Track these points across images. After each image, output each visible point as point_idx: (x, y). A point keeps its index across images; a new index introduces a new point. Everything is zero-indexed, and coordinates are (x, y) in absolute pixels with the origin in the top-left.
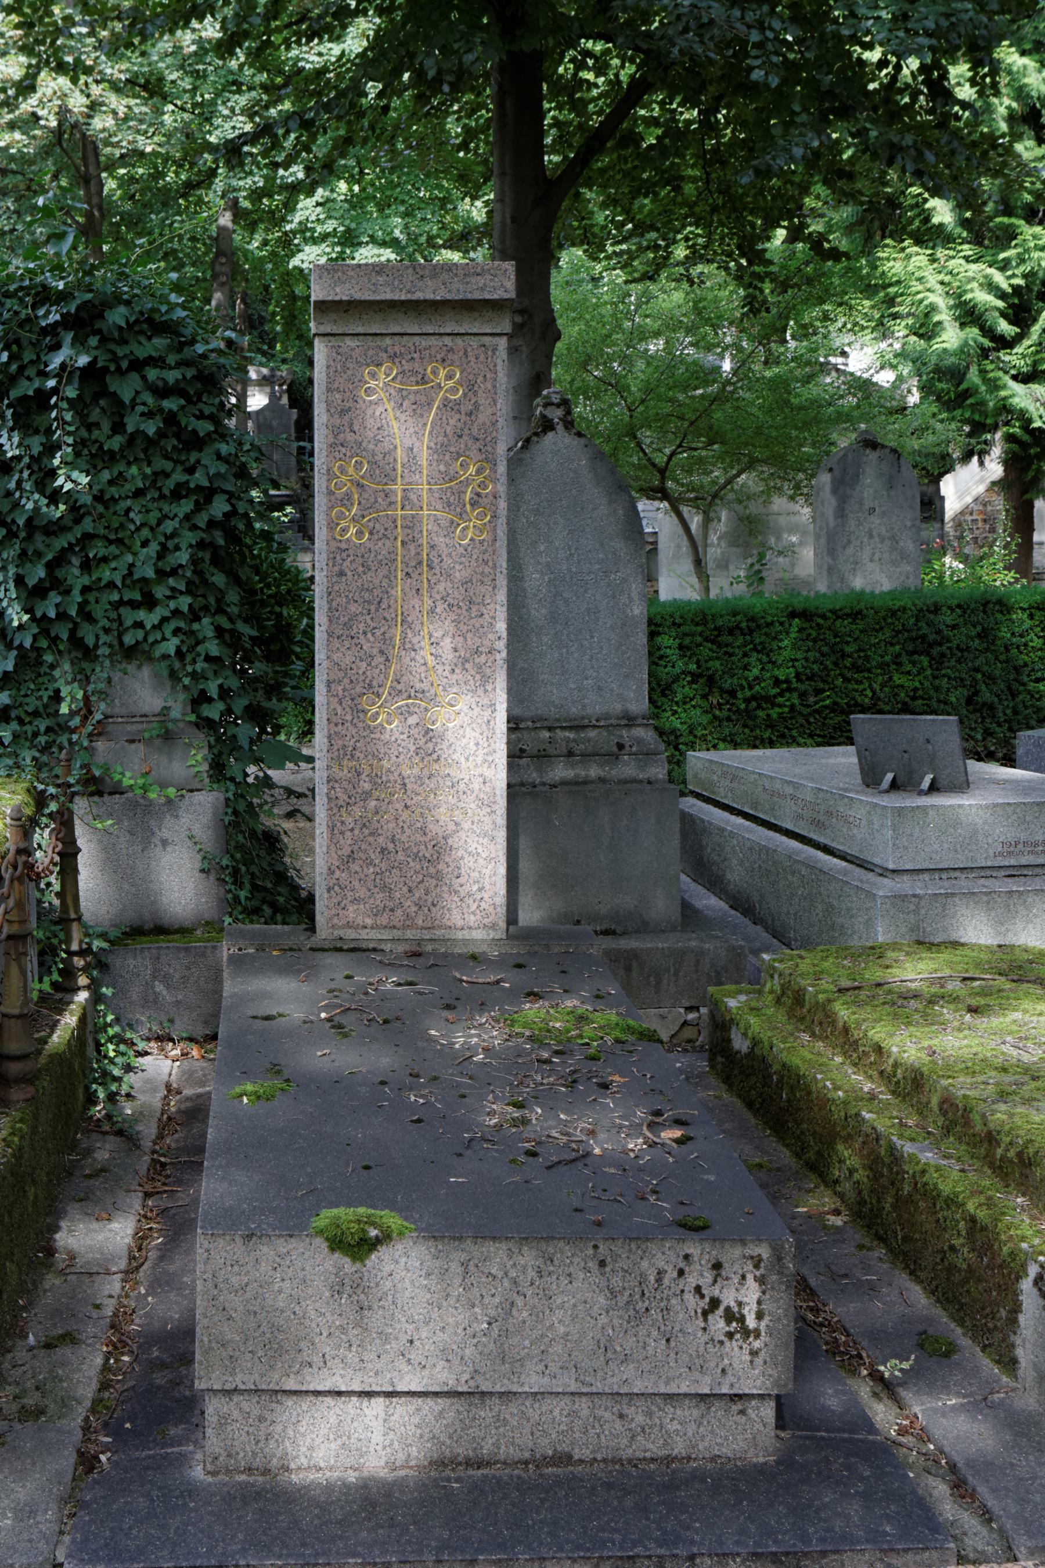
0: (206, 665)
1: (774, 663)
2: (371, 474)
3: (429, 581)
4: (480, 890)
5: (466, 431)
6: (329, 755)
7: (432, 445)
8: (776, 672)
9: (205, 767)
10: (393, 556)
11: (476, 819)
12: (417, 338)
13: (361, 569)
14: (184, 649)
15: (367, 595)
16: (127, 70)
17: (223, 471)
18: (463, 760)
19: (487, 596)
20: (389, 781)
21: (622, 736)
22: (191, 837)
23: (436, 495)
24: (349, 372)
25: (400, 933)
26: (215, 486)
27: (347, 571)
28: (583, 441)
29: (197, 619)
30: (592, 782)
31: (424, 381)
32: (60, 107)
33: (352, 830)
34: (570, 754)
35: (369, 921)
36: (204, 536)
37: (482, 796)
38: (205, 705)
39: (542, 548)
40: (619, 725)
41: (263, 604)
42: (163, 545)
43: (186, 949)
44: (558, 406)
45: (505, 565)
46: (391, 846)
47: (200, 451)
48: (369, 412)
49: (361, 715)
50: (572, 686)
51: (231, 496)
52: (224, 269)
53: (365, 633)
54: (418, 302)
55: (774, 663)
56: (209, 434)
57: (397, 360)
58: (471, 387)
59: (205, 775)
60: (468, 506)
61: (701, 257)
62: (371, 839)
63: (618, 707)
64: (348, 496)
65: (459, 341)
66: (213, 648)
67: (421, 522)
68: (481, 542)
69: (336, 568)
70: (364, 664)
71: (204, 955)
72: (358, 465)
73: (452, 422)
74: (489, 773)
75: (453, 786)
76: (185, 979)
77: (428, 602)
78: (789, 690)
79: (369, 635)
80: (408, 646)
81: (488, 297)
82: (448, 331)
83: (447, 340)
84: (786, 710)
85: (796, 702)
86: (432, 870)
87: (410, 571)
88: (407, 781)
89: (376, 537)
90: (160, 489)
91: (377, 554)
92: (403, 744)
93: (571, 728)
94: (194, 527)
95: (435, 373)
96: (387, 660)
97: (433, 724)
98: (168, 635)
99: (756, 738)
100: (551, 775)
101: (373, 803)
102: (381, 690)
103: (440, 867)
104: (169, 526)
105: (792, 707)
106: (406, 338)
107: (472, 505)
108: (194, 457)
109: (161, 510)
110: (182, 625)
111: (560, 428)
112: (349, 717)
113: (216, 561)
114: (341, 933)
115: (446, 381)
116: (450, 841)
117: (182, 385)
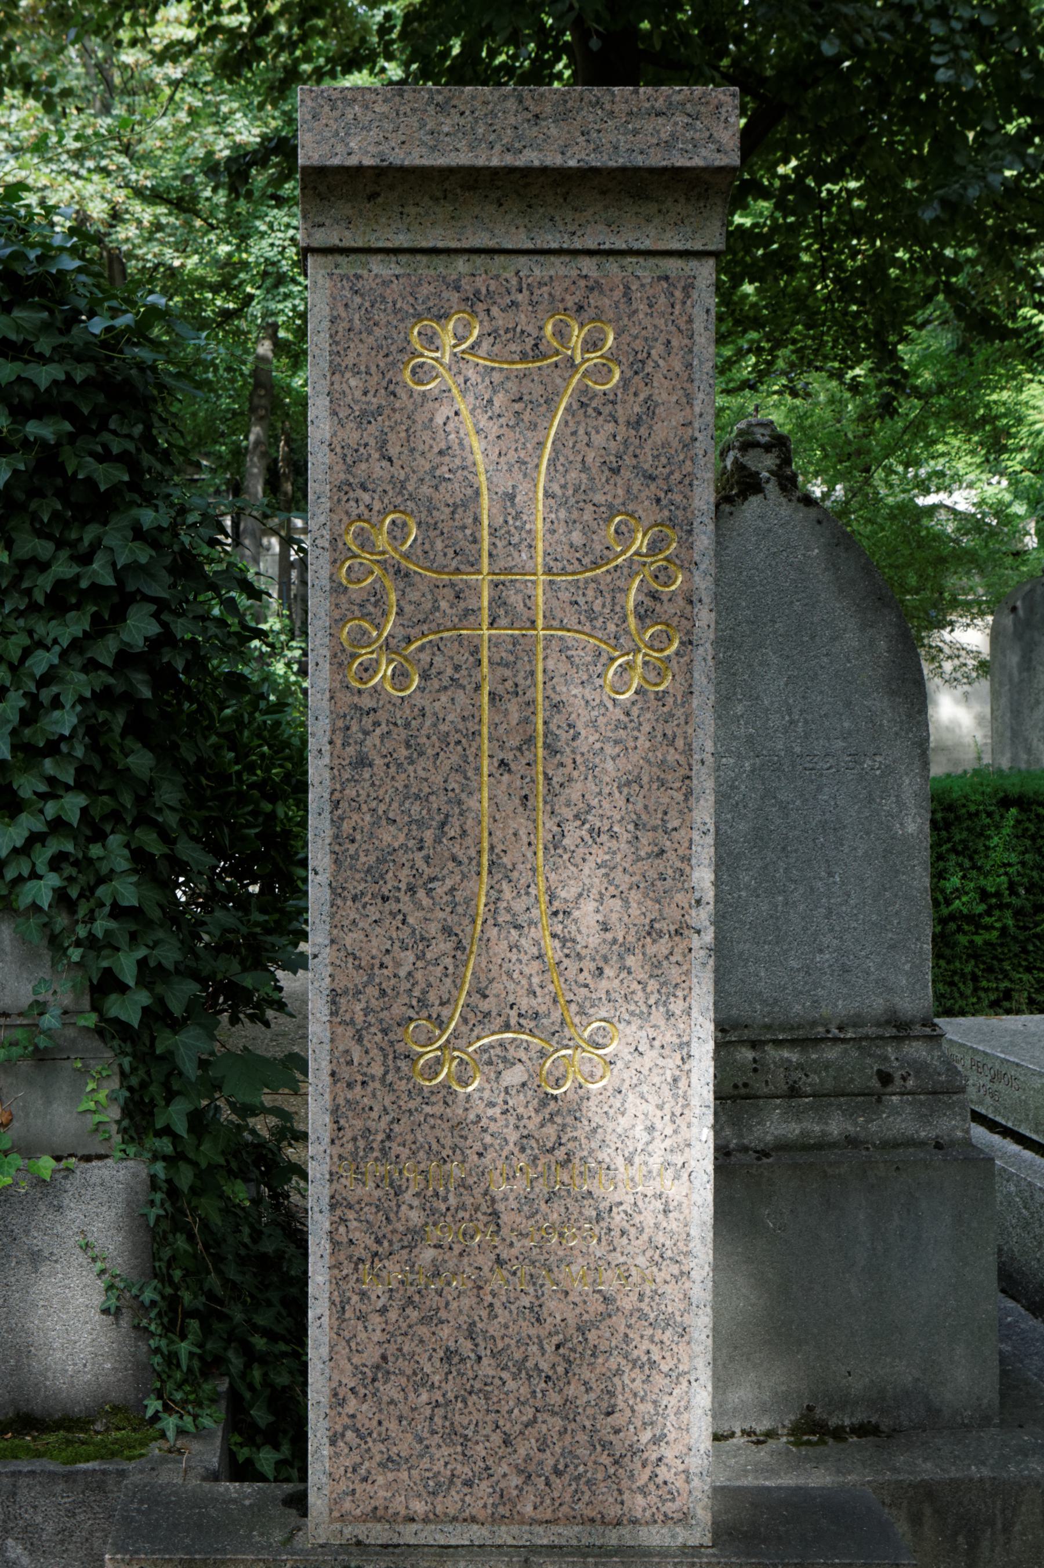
0: (112, 925)
1: (979, 869)
2: (424, 552)
3: (548, 778)
4: (656, 1440)
5: (628, 460)
6: (336, 1150)
7: (556, 488)
8: (983, 882)
9: (115, 1113)
10: (472, 726)
11: (648, 1288)
12: (523, 260)
13: (403, 752)
14: (74, 893)
15: (416, 808)
16: (154, 176)
17: (143, 560)
18: (620, 1162)
19: (673, 813)
20: (463, 1207)
21: (886, 1059)
22: (87, 1247)
23: (565, 596)
24: (378, 332)
25: (485, 1532)
26: (131, 587)
27: (373, 755)
28: (813, 512)
29: (99, 836)
30: (834, 1145)
31: (537, 351)
32: (77, 212)
33: (383, 1311)
34: (794, 1092)
35: (419, 1507)
36: (111, 681)
37: (660, 1239)
38: (113, 997)
39: (739, 709)
40: (881, 1038)
41: (242, 798)
42: (33, 698)
43: (68, 1477)
44: (768, 448)
45: (709, 746)
46: (466, 1346)
47: (105, 523)
48: (421, 417)
49: (403, 1064)
50: (794, 964)
51: (161, 607)
52: (263, 402)
53: (411, 889)
54: (527, 172)
55: (979, 869)
56: (115, 490)
57: (480, 307)
58: (638, 366)
59: (114, 1128)
60: (632, 621)
61: (810, 364)
62: (423, 1331)
63: (877, 1004)
64: (377, 596)
65: (612, 266)
66: (127, 891)
67: (531, 653)
68: (660, 697)
69: (351, 750)
70: (410, 956)
71: (101, 1488)
72: (398, 531)
73: (599, 440)
74: (675, 1191)
75: (599, 1218)
76: (65, 1535)
77: (546, 826)
78: (1001, 906)
79: (421, 894)
80: (503, 917)
81: (681, 162)
82: (591, 245)
83: (588, 265)
84: (995, 933)
85: (1010, 922)
86: (554, 1398)
87: (509, 756)
88: (500, 1207)
89: (436, 684)
90: (29, 592)
91: (438, 720)
92: (493, 1127)
93: (793, 1043)
94: (92, 666)
95: (561, 334)
96: (459, 947)
97: (558, 1085)
98: (41, 869)
99: (955, 973)
100: (758, 1132)
101: (429, 1254)
102: (445, 1012)
103: (571, 1391)
104: (41, 662)
105: (1004, 930)
106: (500, 259)
107: (640, 617)
108: (90, 534)
109: (30, 633)
110: (69, 847)
111: (772, 488)
112: (377, 1070)
113: (139, 728)
114: (360, 1531)
115: (586, 351)
116: (592, 1336)
117: (68, 396)
